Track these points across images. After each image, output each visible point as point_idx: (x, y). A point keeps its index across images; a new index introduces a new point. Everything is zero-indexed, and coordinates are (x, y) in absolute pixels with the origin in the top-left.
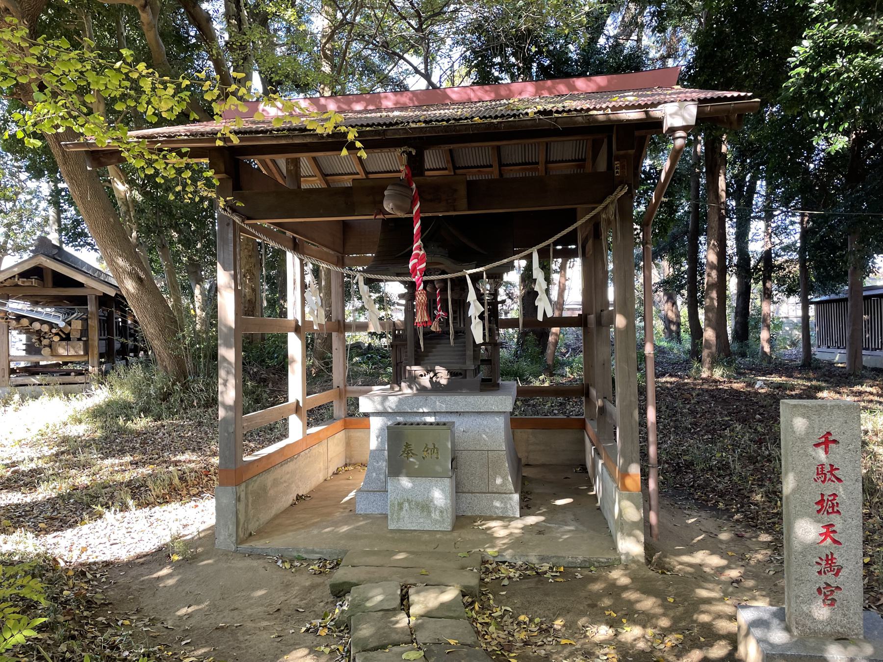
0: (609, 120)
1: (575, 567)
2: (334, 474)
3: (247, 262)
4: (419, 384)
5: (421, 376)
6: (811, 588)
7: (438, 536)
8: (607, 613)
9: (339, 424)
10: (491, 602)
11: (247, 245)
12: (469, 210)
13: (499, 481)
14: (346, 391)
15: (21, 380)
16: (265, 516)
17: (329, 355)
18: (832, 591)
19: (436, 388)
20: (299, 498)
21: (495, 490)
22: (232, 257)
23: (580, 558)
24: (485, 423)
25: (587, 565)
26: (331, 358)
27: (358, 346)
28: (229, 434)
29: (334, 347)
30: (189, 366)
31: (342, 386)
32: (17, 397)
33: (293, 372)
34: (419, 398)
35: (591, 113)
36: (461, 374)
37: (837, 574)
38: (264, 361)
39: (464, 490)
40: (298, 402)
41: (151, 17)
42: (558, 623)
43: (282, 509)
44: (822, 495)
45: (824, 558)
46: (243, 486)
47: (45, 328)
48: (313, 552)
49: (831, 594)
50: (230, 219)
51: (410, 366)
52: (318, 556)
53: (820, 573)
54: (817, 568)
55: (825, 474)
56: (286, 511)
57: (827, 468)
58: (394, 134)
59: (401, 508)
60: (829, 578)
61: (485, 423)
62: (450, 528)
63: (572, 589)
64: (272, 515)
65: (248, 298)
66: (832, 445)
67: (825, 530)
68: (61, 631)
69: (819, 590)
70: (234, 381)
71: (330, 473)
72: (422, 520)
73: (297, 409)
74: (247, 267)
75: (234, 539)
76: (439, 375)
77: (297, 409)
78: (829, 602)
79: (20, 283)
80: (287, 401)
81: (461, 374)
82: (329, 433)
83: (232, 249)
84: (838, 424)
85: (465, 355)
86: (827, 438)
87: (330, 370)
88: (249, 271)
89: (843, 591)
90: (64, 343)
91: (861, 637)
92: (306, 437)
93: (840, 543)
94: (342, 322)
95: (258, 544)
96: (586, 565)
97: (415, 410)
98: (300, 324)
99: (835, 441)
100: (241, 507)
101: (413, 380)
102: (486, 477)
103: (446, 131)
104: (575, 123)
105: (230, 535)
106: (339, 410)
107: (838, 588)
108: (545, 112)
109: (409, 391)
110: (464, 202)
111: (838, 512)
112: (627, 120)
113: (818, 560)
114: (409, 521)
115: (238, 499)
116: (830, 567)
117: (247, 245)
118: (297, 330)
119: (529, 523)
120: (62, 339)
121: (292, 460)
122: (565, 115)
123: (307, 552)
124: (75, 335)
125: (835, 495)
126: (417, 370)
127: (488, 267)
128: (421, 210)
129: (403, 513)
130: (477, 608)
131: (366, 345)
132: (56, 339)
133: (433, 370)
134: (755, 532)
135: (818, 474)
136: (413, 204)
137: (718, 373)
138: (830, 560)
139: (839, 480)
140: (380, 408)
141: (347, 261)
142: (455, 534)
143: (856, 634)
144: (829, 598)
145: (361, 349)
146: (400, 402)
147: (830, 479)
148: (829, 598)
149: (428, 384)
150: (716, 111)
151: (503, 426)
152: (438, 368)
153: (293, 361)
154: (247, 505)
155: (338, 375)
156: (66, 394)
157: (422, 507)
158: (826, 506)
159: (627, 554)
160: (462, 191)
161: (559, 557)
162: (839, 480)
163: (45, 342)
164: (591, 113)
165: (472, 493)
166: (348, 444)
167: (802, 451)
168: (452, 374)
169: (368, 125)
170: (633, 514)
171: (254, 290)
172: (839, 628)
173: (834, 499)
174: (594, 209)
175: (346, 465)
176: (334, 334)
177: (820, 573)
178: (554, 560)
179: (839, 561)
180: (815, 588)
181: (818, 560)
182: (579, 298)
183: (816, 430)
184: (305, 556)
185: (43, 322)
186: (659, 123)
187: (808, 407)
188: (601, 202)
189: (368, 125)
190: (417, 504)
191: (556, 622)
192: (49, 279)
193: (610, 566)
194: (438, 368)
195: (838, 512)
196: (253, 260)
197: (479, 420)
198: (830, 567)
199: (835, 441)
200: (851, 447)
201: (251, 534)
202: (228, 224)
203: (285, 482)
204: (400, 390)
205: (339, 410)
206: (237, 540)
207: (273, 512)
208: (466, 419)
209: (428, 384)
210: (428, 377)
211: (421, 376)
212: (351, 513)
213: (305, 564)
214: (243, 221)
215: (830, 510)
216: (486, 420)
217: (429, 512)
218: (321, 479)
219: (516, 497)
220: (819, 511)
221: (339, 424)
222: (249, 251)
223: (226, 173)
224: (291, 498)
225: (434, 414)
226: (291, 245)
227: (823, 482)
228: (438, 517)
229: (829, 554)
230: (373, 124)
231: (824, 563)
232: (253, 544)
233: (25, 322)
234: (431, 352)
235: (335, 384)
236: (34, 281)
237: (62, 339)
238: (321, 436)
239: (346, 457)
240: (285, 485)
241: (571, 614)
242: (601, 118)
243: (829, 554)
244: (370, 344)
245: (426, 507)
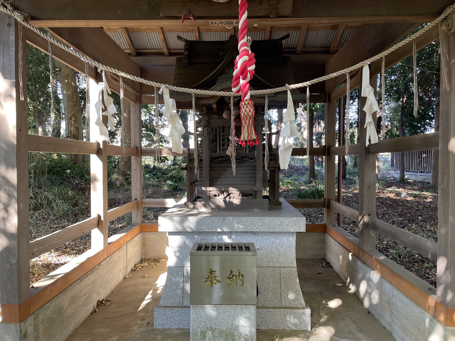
2: (132, 270)
3: (72, 110)
4: (214, 203)
5: (215, 196)
9: (136, 229)
11: (72, 97)
13: (291, 296)
14: (142, 203)
17: (129, 172)
19: (230, 207)
20: (100, 303)
21: (287, 305)
22: (13, 63)
26: (129, 175)
27: (147, 167)
28: (11, 265)
29: (133, 168)
31: (139, 199)
33: (95, 189)
34: (216, 219)
36: (251, 195)
38: (83, 176)
40: (99, 217)
46: (30, 320)
50: (10, 17)
51: (206, 187)
56: (86, 323)
61: (278, 241)
64: (70, 333)
65: (73, 133)
70: (16, 206)
71: (129, 270)
73: (99, 223)
74: (72, 113)
76: (231, 195)
77: (99, 223)
80: (90, 216)
82: (128, 238)
83: (13, 53)
85: (255, 177)
87: (129, 184)
88: (74, 115)
92: (108, 245)
94: (139, 148)
97: (214, 230)
98: (101, 147)
101: (207, 199)
102: (279, 292)
106: (137, 218)
109: (203, 210)
117: (72, 97)
118: (99, 152)
121: (93, 272)
126: (212, 190)
131: (152, 166)
133: (227, 191)
140: (179, 228)
141: (143, 99)
145: (149, 169)
146: (199, 223)
149: (222, 204)
151: (294, 244)
153: (96, 179)
155: (136, 190)
157: (226, 335)
165: (266, 308)
166: (144, 244)
168: (244, 194)
171: (77, 129)
175: (142, 261)
176: (133, 158)
182: (280, 138)
188: (440, 14)
190: (221, 333)
194: (231, 189)
196: (77, 108)
197: (272, 239)
204: (194, 208)
205: (137, 218)
209: (222, 204)
210: (222, 197)
211: (215, 196)
212: (149, 328)
214: (26, 20)
216: (279, 237)
218: (121, 277)
219: (308, 311)
221: (136, 229)
222: (73, 102)
225: (230, 234)
234: (222, 174)
235: (133, 198)
238: (121, 242)
239: (142, 254)
240: (85, 297)
244: (154, 166)
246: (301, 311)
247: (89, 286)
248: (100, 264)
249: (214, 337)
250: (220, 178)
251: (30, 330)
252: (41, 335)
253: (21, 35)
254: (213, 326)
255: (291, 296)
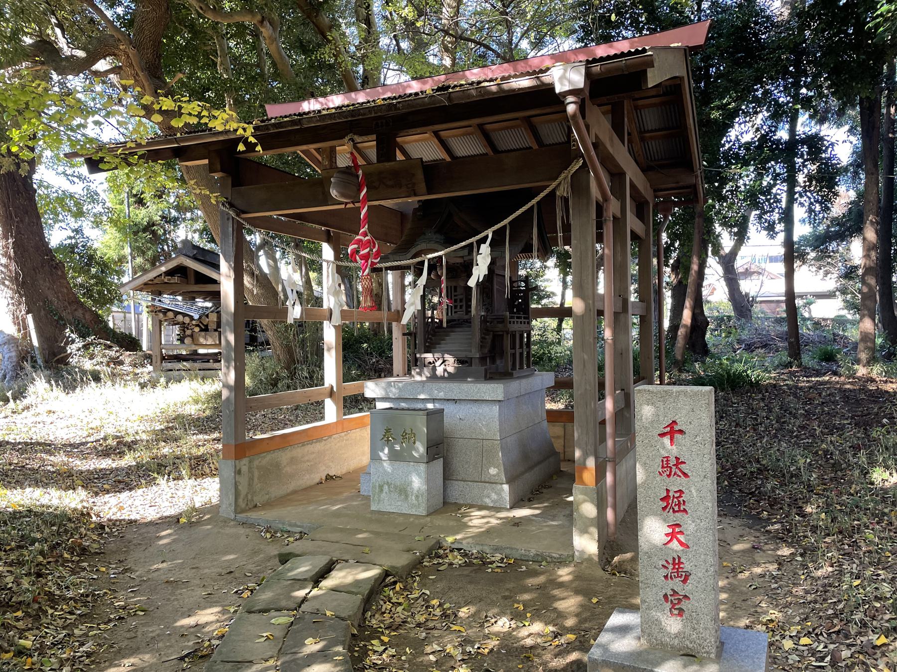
0: (501, 90)
1: (528, 561)
6: (657, 594)
7: (412, 520)
8: (516, 605)
10: (416, 584)
12: (429, 194)
15: (169, 365)
16: (276, 491)
18: (680, 600)
20: (329, 478)
21: (487, 480)
23: (533, 552)
24: (481, 411)
25: (540, 559)
30: (299, 353)
32: (163, 380)
35: (483, 84)
36: (466, 362)
37: (685, 581)
38: (384, 352)
39: (458, 478)
40: (332, 387)
41: (271, 31)
42: (464, 612)
43: (304, 486)
44: (668, 491)
45: (671, 561)
46: (245, 461)
47: (187, 320)
48: (296, 526)
49: (679, 603)
52: (299, 529)
53: (666, 577)
54: (664, 572)
55: (671, 468)
57: (673, 461)
58: (309, 122)
59: (381, 491)
60: (676, 584)
61: (481, 411)
62: (424, 513)
63: (500, 577)
65: (375, 292)
66: (677, 436)
67: (670, 531)
68: (26, 568)
69: (665, 596)
72: (399, 503)
75: (233, 508)
77: (331, 394)
78: (676, 612)
79: (166, 281)
81: (466, 362)
84: (684, 412)
86: (672, 428)
89: (692, 601)
90: (203, 333)
91: (713, 656)
93: (688, 547)
95: (254, 515)
96: (538, 559)
99: (681, 432)
100: (243, 481)
103: (352, 116)
104: (469, 96)
105: (230, 504)
107: (686, 597)
108: (444, 88)
110: (422, 186)
111: (685, 511)
112: (519, 89)
113: (665, 563)
114: (388, 504)
115: (238, 472)
116: (678, 572)
119: (517, 516)
120: (202, 330)
122: (458, 89)
123: (290, 525)
124: (212, 326)
125: (681, 491)
127: (448, 250)
128: (368, 198)
129: (383, 495)
130: (398, 588)
132: (197, 329)
134: (777, 544)
135: (663, 467)
136: (360, 191)
137: (877, 371)
138: (677, 563)
139: (686, 475)
142: (428, 519)
143: (707, 653)
144: (677, 607)
147: (675, 474)
148: (677, 607)
150: (609, 71)
152: (446, 356)
154: (251, 479)
156: (203, 379)
157: (400, 491)
158: (672, 503)
159: (582, 552)
160: (420, 175)
161: (512, 549)
162: (686, 475)
163: (188, 332)
164: (483, 84)
167: (647, 441)
168: (460, 361)
169: (286, 117)
170: (589, 510)
172: (688, 642)
173: (680, 496)
174: (548, 186)
177: (666, 577)
178: (508, 552)
179: (687, 566)
180: (661, 594)
181: (665, 563)
183: (661, 418)
184: (289, 529)
185: (184, 315)
186: (550, 88)
187: (653, 392)
189: (286, 117)
190: (396, 487)
191: (462, 610)
192: (192, 278)
193: (562, 562)
195: (685, 511)
198: (678, 572)
199: (681, 432)
200: (698, 439)
201: (256, 506)
202: (228, 219)
203: (308, 461)
206: (235, 509)
207: (292, 487)
208: (463, 407)
213: (286, 536)
214: (238, 215)
215: (676, 508)
217: (407, 496)
220: (664, 509)
223: (222, 171)
224: (320, 475)
225: (434, 400)
226: (325, 237)
227: (669, 476)
228: (415, 502)
229: (676, 557)
230: (290, 115)
231: (671, 567)
232: (249, 514)
233: (170, 315)
234: (444, 340)
236: (176, 279)
237: (202, 330)
241: (482, 603)
242: (494, 89)
243: (676, 557)
245: (403, 491)
246: (499, 486)
247: (314, 455)
248: (330, 436)
249: (390, 491)
250: (439, 344)
251: (245, 469)
252: (256, 480)
253: (235, 226)
254: (390, 481)
255: (493, 471)
